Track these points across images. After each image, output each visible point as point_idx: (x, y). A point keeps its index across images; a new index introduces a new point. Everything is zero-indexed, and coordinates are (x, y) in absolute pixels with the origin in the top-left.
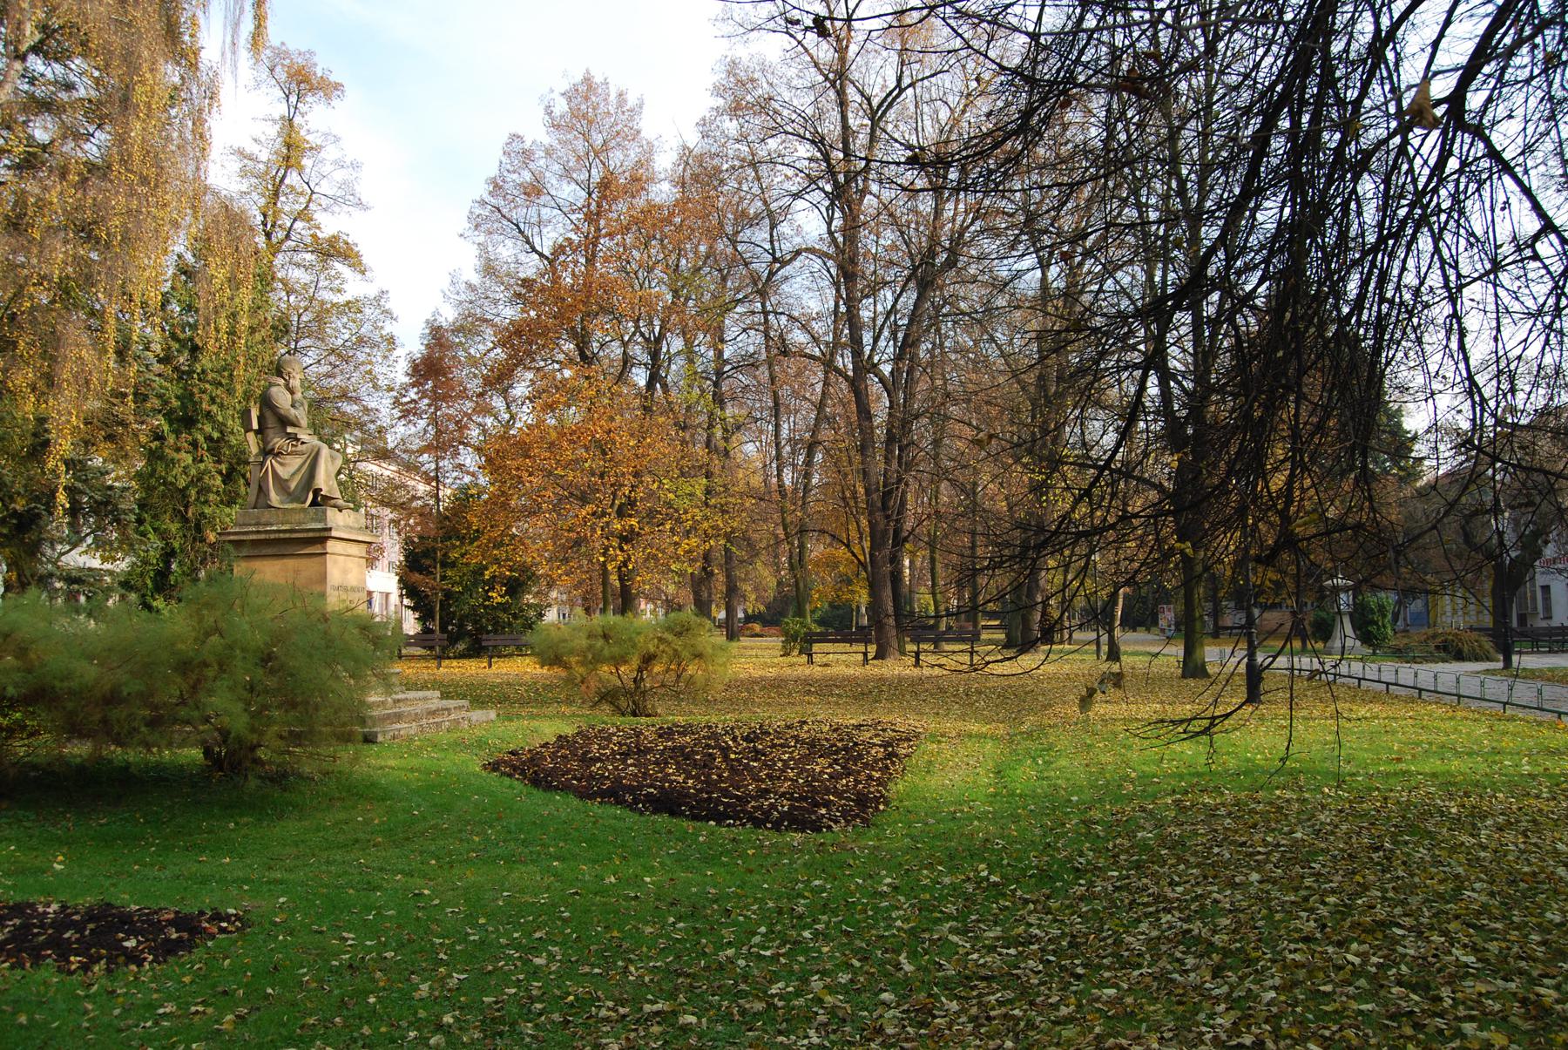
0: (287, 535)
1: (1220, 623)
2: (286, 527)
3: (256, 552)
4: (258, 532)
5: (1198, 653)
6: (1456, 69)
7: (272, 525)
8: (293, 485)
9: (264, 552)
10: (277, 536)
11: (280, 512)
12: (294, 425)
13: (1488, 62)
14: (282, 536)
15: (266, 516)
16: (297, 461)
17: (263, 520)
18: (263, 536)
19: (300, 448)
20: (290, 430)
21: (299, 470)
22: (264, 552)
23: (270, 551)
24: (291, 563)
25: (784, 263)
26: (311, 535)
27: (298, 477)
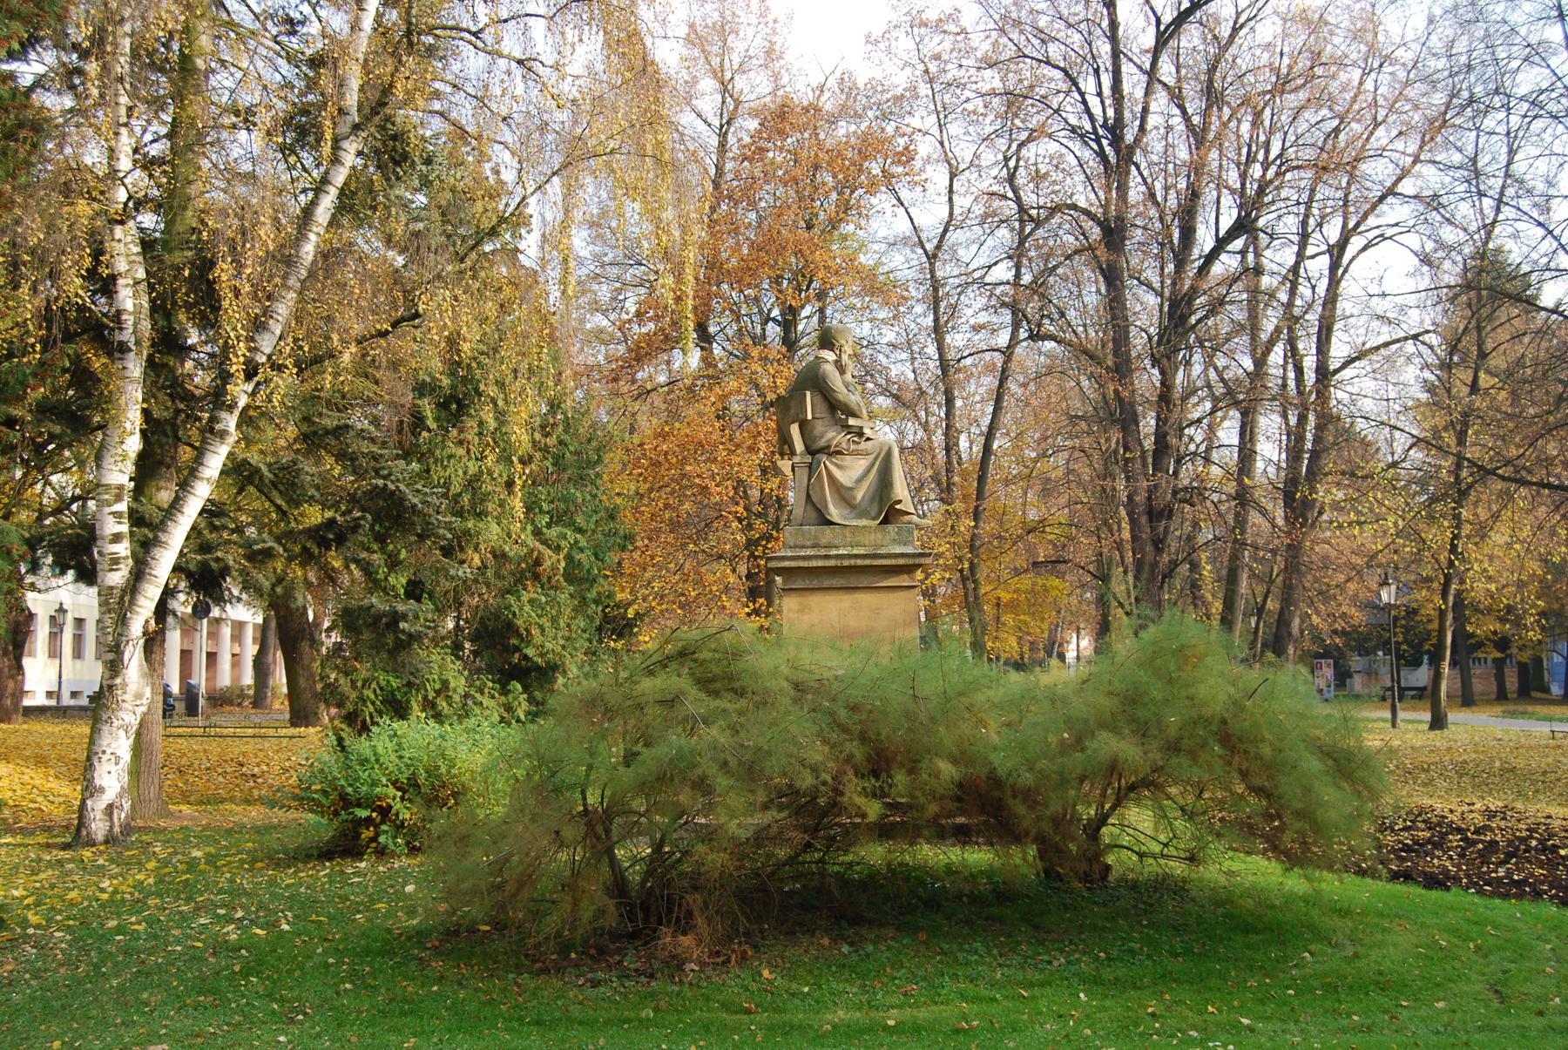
0: (868, 562)
1: (1403, 684)
2: (862, 551)
3: (815, 584)
4: (827, 557)
5: (1432, 673)
6: (1229, 252)
7: (837, 547)
8: (859, 495)
9: (826, 583)
10: (852, 562)
11: (847, 532)
12: (855, 415)
13: (1286, 518)
14: (860, 562)
15: (827, 534)
16: (860, 465)
17: (824, 541)
18: (832, 563)
19: (864, 446)
20: (851, 422)
21: (868, 471)
22: (826, 583)
23: (835, 582)
24: (865, 599)
25: (1038, 223)
26: (901, 561)
27: (865, 485)
